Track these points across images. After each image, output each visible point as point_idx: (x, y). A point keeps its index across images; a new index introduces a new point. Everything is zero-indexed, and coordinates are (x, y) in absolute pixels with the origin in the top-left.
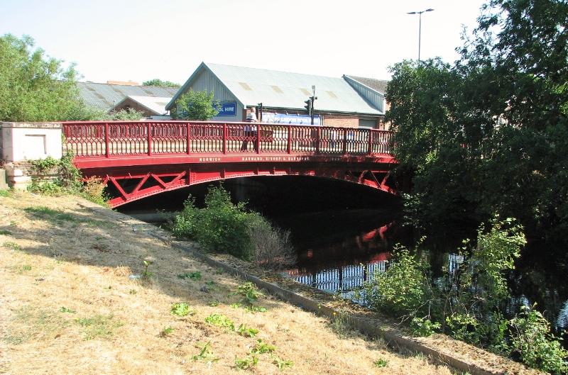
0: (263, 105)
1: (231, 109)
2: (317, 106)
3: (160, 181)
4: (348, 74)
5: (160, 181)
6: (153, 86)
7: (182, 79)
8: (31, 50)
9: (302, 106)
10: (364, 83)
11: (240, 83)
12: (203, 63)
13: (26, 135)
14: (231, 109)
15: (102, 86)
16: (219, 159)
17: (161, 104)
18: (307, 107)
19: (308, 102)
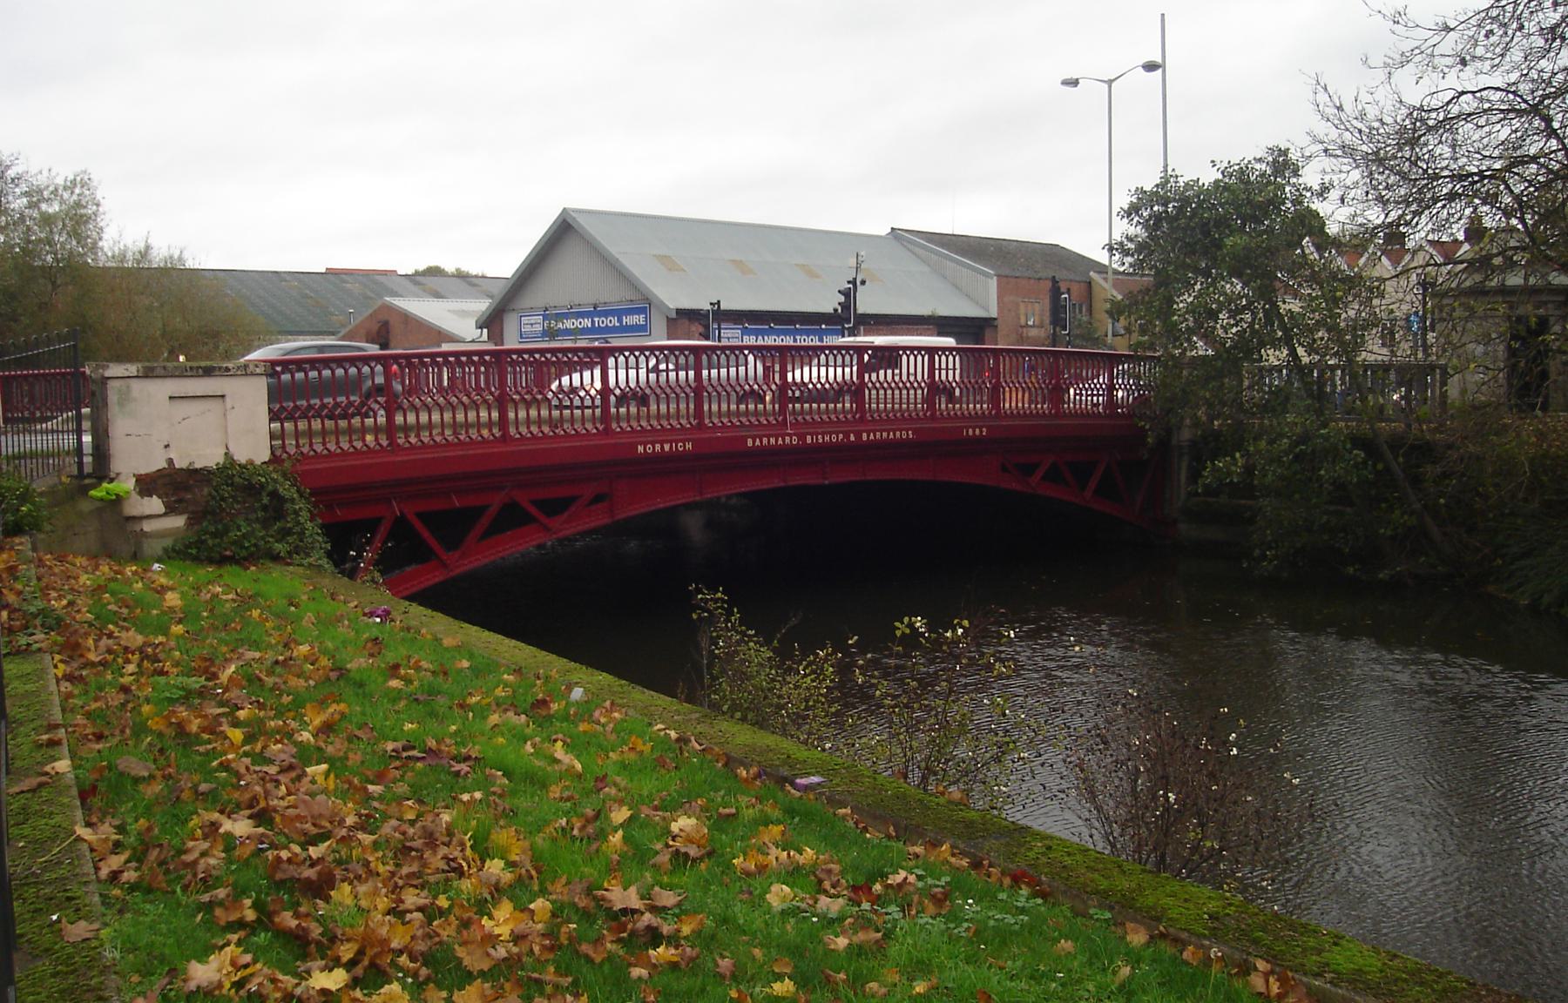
0: (723, 307)
1: (637, 319)
2: (866, 303)
3: (534, 511)
4: (170, 394)
5: (534, 511)
6: (430, 280)
7: (505, 264)
8: (91, 210)
9: (829, 303)
10: (942, 245)
11: (449, 311)
12: (564, 209)
13: (1163, 15)
14: (637, 319)
15: (302, 276)
16: (689, 446)
17: (463, 314)
18: (846, 306)
19: (846, 293)
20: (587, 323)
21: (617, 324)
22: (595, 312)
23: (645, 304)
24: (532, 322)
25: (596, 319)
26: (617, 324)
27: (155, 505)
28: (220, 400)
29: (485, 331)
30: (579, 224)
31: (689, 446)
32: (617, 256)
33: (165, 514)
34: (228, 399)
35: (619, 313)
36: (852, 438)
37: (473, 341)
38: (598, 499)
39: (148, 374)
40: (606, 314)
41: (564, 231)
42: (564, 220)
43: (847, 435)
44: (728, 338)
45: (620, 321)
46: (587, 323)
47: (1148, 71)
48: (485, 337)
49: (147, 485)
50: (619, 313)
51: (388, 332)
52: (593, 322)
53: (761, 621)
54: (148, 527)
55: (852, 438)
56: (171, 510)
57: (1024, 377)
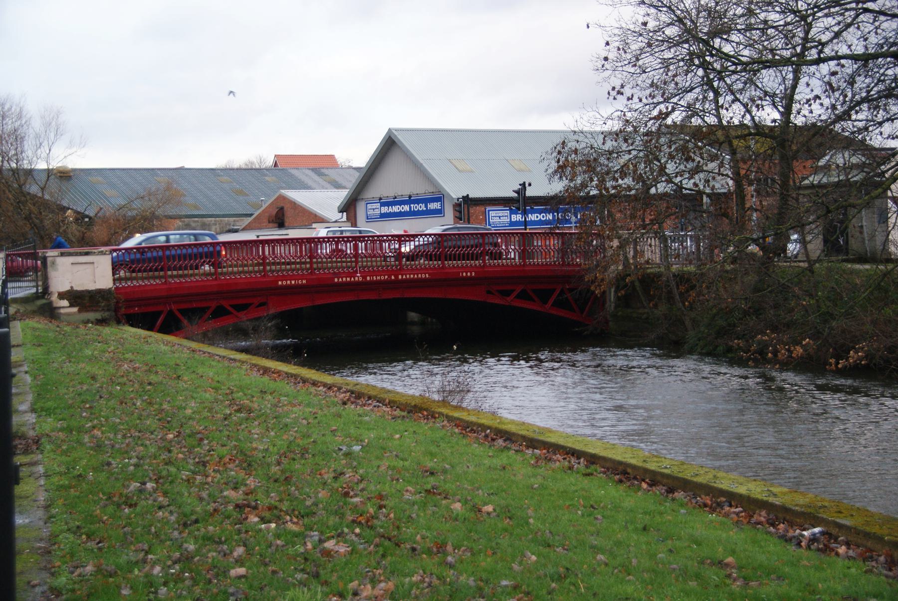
12: (390, 130)
20: (406, 208)
21: (425, 209)
22: (410, 201)
23: (439, 197)
24: (374, 207)
25: (412, 205)
26: (425, 209)
27: (65, 303)
28: (91, 266)
29: (345, 213)
30: (399, 140)
31: (304, 282)
32: (422, 162)
33: (70, 307)
34: (95, 264)
35: (426, 201)
36: (393, 277)
37: (336, 222)
38: (261, 305)
39: (62, 254)
40: (417, 202)
41: (390, 145)
42: (390, 137)
43: (390, 276)
44: (500, 217)
45: (426, 206)
46: (406, 208)
47: (332, 157)
48: (345, 219)
49: (62, 296)
50: (426, 201)
51: (283, 215)
52: (410, 208)
53: (190, 320)
54: (62, 311)
55: (393, 277)
56: (71, 305)
57: (247, 253)
